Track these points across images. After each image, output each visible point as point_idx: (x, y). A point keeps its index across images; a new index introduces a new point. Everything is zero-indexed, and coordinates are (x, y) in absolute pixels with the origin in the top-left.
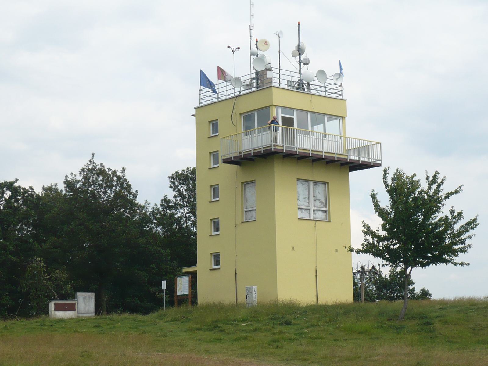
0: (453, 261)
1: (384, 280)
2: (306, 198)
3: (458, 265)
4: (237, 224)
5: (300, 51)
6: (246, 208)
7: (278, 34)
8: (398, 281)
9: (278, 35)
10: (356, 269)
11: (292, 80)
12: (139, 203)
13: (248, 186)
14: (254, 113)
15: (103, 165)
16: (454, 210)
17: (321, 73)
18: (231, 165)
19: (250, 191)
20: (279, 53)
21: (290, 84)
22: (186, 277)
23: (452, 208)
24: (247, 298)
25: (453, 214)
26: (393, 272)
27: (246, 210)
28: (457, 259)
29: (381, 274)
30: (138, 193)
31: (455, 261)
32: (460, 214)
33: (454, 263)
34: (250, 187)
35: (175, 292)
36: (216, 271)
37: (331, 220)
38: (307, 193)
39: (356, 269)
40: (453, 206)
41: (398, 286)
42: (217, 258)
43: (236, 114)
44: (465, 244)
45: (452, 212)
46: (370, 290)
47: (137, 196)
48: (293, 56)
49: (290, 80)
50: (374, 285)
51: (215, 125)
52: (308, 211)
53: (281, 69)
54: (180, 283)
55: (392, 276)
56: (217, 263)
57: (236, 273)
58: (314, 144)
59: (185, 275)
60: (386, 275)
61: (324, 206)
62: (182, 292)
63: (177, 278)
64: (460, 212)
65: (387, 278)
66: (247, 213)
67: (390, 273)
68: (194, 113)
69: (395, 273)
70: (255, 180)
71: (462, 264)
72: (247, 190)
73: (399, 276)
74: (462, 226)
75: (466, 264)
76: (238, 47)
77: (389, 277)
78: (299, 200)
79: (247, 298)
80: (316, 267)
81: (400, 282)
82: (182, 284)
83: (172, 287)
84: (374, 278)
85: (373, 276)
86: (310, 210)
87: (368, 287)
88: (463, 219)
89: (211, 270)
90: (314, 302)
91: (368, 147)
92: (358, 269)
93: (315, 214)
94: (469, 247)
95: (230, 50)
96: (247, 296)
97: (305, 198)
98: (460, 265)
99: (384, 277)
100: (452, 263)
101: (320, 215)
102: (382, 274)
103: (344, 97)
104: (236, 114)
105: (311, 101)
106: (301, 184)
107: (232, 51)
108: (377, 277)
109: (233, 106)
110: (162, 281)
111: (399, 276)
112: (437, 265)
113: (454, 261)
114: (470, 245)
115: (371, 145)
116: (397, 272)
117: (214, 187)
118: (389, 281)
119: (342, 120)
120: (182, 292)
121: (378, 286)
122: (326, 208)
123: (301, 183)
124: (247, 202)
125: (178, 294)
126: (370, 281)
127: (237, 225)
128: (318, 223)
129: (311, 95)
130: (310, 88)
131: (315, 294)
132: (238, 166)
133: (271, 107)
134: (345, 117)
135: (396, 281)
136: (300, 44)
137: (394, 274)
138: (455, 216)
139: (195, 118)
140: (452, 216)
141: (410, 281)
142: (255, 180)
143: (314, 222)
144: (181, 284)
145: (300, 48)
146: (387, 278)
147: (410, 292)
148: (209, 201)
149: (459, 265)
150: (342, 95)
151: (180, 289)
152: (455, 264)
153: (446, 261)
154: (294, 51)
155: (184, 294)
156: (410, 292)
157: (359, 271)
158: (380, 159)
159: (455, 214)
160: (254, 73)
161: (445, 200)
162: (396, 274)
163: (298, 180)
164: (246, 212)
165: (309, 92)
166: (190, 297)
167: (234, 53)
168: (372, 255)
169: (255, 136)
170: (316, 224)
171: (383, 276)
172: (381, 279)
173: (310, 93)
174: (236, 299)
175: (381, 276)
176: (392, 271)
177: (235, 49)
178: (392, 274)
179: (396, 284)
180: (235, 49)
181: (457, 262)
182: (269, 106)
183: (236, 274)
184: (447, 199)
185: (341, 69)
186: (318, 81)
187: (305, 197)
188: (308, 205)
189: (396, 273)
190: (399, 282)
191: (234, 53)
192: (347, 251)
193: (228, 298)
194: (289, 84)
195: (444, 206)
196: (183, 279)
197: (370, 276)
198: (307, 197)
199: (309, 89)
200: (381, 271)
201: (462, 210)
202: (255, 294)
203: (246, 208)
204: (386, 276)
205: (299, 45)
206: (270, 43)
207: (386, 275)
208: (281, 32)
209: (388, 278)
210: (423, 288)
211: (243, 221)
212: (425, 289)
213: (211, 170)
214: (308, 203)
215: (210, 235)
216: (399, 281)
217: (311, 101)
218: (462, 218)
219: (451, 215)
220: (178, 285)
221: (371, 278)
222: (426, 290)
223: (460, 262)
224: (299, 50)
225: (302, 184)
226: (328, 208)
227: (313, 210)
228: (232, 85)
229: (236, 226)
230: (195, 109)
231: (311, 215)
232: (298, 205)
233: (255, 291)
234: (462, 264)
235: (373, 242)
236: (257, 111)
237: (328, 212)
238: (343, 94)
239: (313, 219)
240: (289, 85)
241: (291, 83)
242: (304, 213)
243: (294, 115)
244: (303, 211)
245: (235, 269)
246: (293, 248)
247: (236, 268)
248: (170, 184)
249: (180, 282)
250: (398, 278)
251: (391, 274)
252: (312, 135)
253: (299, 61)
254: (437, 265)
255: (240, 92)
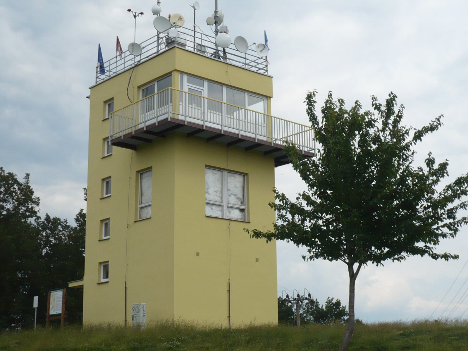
0: (431, 252)
1: (321, 310)
2: (218, 191)
3: (440, 258)
4: (130, 224)
5: (217, 20)
6: (141, 203)
7: (193, 6)
8: (334, 311)
9: (194, 7)
10: (292, 296)
11: (203, 44)
12: (71, 226)
13: (145, 175)
14: (155, 84)
15: (3, 169)
16: (433, 158)
17: (241, 40)
18: (124, 149)
19: (147, 183)
20: (195, 27)
21: (199, 48)
22: (59, 292)
23: (430, 156)
24: (133, 320)
25: (432, 166)
26: (329, 303)
27: (141, 206)
28: (438, 249)
29: (318, 305)
30: (39, 200)
31: (434, 252)
32: (443, 166)
33: (433, 254)
34: (146, 177)
35: (47, 312)
36: (104, 285)
37: (250, 221)
38: (219, 186)
39: (292, 296)
40: (430, 153)
41: (334, 316)
42: (105, 267)
43: (133, 87)
44: (454, 218)
45: (430, 162)
46: (307, 320)
47: (39, 204)
48: (208, 24)
49: (201, 44)
50: (312, 316)
51: (109, 103)
52: (220, 208)
53: (196, 42)
54: (53, 300)
55: (329, 307)
56: (106, 275)
57: (125, 287)
58: (231, 122)
59: (60, 289)
60: (323, 305)
61: (242, 203)
62: (54, 311)
63: (51, 292)
64: (444, 163)
65: (324, 309)
66: (143, 210)
67: (326, 304)
68: (88, 94)
69: (331, 304)
70: (151, 167)
71: (446, 257)
72: (144, 180)
73: (335, 307)
74: (449, 187)
75: (452, 257)
76: (141, 12)
77: (325, 308)
78: (209, 194)
79: (133, 320)
80: (229, 280)
81: (336, 312)
82: (55, 300)
83: (44, 303)
84: (311, 308)
85: (311, 307)
86: (222, 206)
87: (305, 317)
88: (448, 175)
89: (99, 284)
90: (225, 324)
91: (298, 135)
92: (294, 297)
93: (229, 212)
94: (463, 223)
95: (131, 15)
96: (133, 316)
97: (216, 192)
98: (443, 259)
99: (321, 308)
100: (429, 254)
101: (236, 214)
102: (319, 305)
103: (269, 73)
104: (133, 87)
105: (227, 71)
106: (212, 173)
107: (133, 16)
108: (315, 308)
109: (130, 77)
110: (34, 297)
111: (335, 307)
112: (400, 261)
113: (432, 251)
114: (465, 219)
115: (302, 132)
116: (333, 303)
117: (107, 181)
118: (325, 311)
119: (266, 101)
120: (54, 311)
121: (315, 317)
122: (244, 206)
123: (212, 172)
124: (143, 196)
125: (50, 314)
126: (308, 311)
127: (129, 225)
128: (232, 223)
129: (226, 65)
130: (226, 56)
131: (227, 315)
132: (133, 150)
133: (173, 73)
134: (270, 97)
135: (332, 311)
136: (217, 11)
137: (330, 305)
138: (436, 169)
139: (89, 100)
140: (430, 169)
141: (345, 311)
142: (151, 167)
143: (228, 222)
144: (54, 300)
145: (217, 15)
146: (324, 309)
147: (345, 322)
148: (100, 198)
149: (441, 258)
150: (267, 71)
151: (53, 308)
152: (435, 257)
153: (422, 252)
154: (211, 17)
155: (57, 313)
156: (345, 322)
157: (295, 298)
158: (313, 147)
159: (436, 166)
160: (156, 36)
161: (415, 144)
162: (332, 305)
163: (208, 167)
164: (141, 208)
165: (225, 61)
166: (62, 316)
167: (135, 19)
168: (292, 242)
169: (153, 112)
170: (229, 224)
171: (320, 307)
172: (318, 309)
173: (225, 62)
174: (125, 321)
175: (318, 307)
176: (328, 302)
177: (137, 14)
178: (328, 305)
179: (332, 314)
180: (137, 14)
181: (438, 253)
182: (171, 72)
183: (126, 288)
184: (418, 141)
185: (266, 41)
186: (238, 51)
187: (217, 189)
188: (221, 200)
189: (332, 304)
190: (335, 312)
191: (135, 19)
192: (250, 237)
193: (118, 319)
194: (199, 49)
195: (415, 154)
196: (57, 293)
197: (307, 307)
198: (219, 190)
199: (225, 58)
200: (318, 302)
201: (447, 160)
202: (144, 313)
203: (142, 204)
204: (322, 307)
205: (216, 12)
206: (184, 17)
207: (323, 305)
208: (197, 3)
209: (325, 309)
210: (357, 318)
211: (136, 221)
212: (359, 319)
213: (104, 159)
214: (221, 198)
215: (99, 241)
216: (335, 311)
217: (227, 71)
218: (445, 174)
219: (428, 168)
220: (51, 302)
221: (308, 308)
222: (360, 320)
223: (443, 253)
224: (216, 17)
225: (213, 173)
226: (247, 206)
227: (226, 207)
228: (128, 51)
229: (128, 227)
230: (90, 89)
231: (224, 212)
232: (206, 200)
233: (144, 309)
234: (446, 257)
235: (292, 220)
236: (157, 81)
237: (246, 211)
238: (268, 70)
239: (226, 218)
240: (199, 50)
241: (201, 47)
242: (214, 211)
243: (205, 87)
244: (214, 207)
245: (125, 282)
246: (198, 254)
247: (126, 281)
248: (85, 196)
249: (54, 297)
250: (334, 309)
251: (327, 305)
252: (228, 114)
253: (216, 30)
254: (400, 261)
255: (139, 61)
